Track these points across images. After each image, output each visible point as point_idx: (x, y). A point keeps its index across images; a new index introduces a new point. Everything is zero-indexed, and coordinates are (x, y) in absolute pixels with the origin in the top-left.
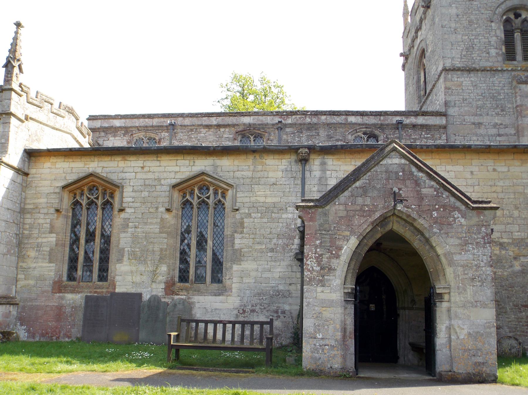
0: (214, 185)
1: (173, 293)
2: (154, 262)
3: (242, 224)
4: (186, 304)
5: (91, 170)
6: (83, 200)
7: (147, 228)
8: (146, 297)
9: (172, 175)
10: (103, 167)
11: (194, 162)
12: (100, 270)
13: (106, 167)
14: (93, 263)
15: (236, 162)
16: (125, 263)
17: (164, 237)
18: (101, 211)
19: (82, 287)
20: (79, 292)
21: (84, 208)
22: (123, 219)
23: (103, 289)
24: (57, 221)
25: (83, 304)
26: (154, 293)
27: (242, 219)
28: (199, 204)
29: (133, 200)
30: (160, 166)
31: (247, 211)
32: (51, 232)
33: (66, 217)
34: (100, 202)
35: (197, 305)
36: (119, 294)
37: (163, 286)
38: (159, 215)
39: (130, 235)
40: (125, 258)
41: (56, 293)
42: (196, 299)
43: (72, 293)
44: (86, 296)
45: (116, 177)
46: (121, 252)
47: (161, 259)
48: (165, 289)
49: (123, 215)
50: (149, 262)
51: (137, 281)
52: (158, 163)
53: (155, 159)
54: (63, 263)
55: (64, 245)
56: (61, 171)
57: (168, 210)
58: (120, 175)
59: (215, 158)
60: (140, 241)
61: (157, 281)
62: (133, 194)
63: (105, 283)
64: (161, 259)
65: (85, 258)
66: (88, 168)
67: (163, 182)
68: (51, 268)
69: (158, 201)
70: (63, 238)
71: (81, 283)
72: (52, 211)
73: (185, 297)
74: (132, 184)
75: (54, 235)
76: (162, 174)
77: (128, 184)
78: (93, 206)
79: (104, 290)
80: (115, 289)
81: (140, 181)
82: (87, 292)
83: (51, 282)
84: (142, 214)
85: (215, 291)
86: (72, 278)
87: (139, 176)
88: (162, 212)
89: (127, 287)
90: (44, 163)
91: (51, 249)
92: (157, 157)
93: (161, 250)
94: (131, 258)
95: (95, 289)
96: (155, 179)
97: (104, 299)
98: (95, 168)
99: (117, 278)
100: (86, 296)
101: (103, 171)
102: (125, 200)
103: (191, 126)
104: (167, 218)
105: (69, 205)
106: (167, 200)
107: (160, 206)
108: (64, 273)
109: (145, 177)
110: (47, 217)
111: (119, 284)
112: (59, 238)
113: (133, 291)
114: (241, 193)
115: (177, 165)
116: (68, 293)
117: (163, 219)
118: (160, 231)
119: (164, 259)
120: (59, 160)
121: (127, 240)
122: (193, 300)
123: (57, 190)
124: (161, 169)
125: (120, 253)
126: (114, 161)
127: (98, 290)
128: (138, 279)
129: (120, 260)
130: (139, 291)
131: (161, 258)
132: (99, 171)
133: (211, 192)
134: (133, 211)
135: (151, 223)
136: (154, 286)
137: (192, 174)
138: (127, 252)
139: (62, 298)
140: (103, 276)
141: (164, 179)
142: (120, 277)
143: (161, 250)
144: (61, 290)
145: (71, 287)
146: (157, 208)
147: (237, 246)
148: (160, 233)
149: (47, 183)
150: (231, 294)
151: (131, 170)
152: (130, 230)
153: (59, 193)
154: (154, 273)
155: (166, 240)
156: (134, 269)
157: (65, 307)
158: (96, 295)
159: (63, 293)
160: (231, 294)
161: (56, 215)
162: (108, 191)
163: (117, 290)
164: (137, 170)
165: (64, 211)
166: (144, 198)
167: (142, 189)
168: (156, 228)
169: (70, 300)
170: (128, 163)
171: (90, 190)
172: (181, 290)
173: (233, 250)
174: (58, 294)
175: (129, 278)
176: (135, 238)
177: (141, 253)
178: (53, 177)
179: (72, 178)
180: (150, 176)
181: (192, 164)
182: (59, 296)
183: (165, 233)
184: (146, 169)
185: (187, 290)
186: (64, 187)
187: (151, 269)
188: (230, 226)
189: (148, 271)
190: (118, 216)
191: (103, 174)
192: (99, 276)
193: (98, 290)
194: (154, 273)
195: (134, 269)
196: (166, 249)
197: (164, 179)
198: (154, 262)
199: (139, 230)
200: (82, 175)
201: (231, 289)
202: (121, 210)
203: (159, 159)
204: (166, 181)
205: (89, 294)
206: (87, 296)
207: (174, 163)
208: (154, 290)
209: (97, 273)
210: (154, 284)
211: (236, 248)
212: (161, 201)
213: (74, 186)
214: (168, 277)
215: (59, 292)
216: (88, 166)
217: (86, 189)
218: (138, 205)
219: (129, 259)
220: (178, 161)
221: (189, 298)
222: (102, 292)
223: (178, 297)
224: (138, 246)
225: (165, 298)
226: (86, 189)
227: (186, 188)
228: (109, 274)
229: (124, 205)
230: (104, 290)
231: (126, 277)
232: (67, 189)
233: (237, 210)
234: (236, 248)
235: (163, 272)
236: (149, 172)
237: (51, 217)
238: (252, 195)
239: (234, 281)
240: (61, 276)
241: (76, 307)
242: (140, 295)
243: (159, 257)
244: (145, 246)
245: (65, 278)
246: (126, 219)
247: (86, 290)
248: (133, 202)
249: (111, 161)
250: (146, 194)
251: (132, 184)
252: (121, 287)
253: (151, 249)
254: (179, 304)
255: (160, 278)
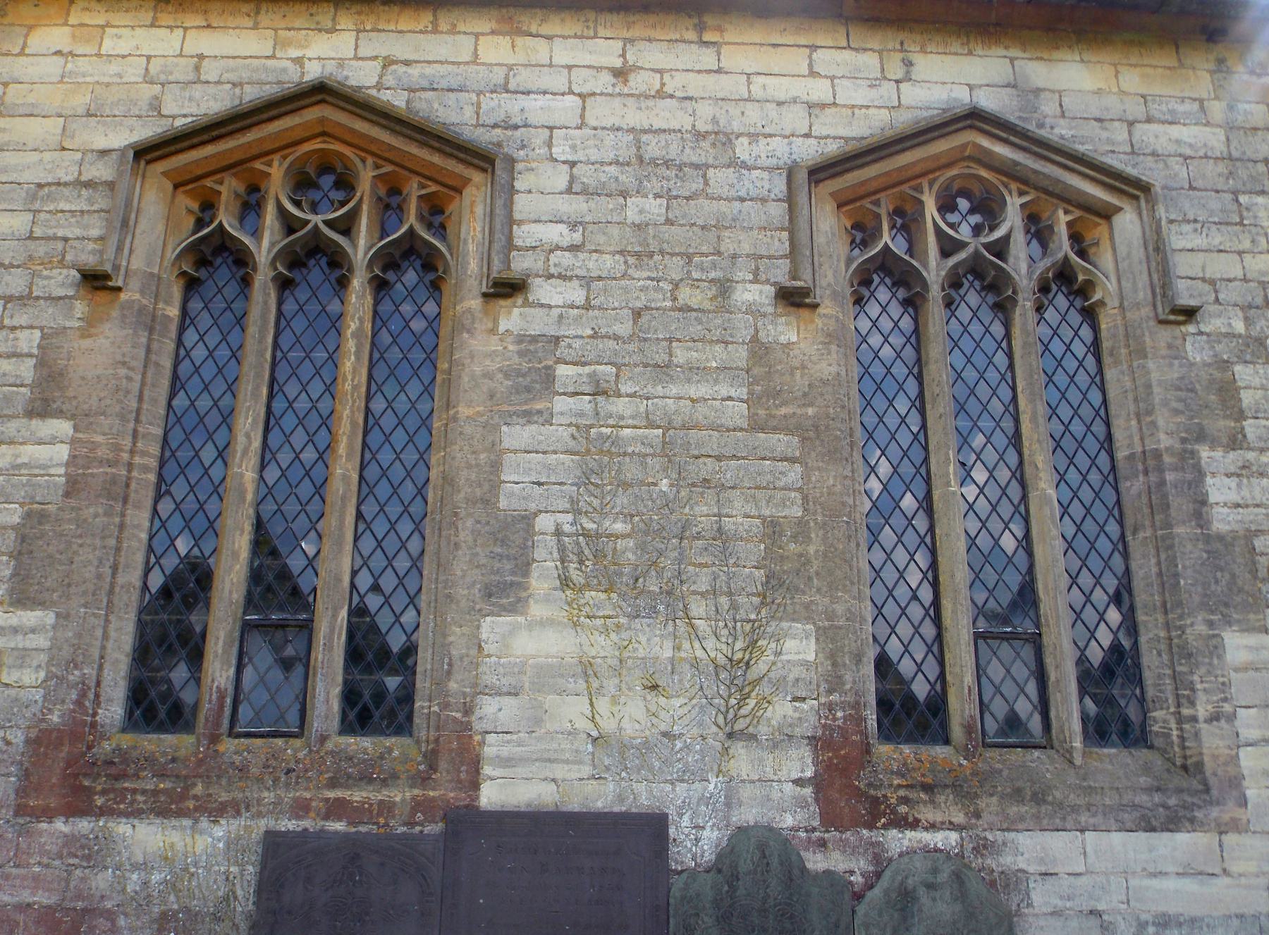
0: (1023, 180)
1: (876, 812)
2: (734, 607)
3: (1228, 391)
4: (974, 886)
5: (313, 72)
6: (256, 234)
7: (672, 397)
8: (696, 841)
9: (795, 119)
10: (388, 62)
11: (909, 64)
12: (354, 655)
13: (407, 63)
14: (309, 608)
15: (1132, 80)
16: (537, 610)
17: (780, 449)
18: (369, 300)
19: (243, 769)
20: (218, 812)
21: (263, 277)
22: (520, 339)
23: (386, 791)
24: (86, 343)
25: (245, 900)
26: (748, 815)
27: (1225, 365)
28: (954, 282)
29: (577, 237)
30: (719, 71)
31: (1239, 327)
32: (41, 408)
33: (150, 322)
34: (361, 248)
35: (1041, 897)
36: (505, 820)
37: (800, 762)
38: (743, 328)
39: (564, 433)
40: (541, 580)
41: (48, 814)
42: (1028, 849)
43: (163, 813)
44: (270, 835)
45: (469, 112)
46: (513, 538)
47: (778, 589)
48: (818, 783)
49: (513, 318)
50: (698, 608)
51: (629, 729)
52: (707, 58)
53: (691, 35)
54: (110, 607)
55: (120, 493)
56: (133, 71)
57: (793, 298)
58: (488, 102)
59: (1014, 52)
60: (632, 471)
61: (763, 731)
62: (576, 206)
63: (395, 745)
64: (778, 589)
65: (255, 576)
66: (299, 61)
67: (743, 149)
68: (19, 641)
69: (728, 246)
70: (117, 448)
71: (228, 746)
72: (61, 281)
73: (954, 837)
74: (561, 151)
75: (63, 427)
76: (735, 111)
77: (543, 151)
78: (316, 273)
79: (400, 795)
80: (475, 786)
81: (610, 138)
82: (276, 809)
83: (18, 737)
84: (637, 314)
85: (1143, 799)
86: (162, 711)
87: (600, 112)
88: (752, 310)
89: (560, 772)
90: (31, 28)
91: (36, 517)
92: (701, 28)
93: (773, 529)
94: (576, 576)
95: (333, 784)
96: (700, 136)
97: (399, 856)
98: (341, 63)
99: (489, 708)
100: (268, 833)
101: (389, 80)
102: (525, 234)
103: (97, 696)
104: (788, 345)
105: (171, 255)
106: (780, 243)
107: (740, 275)
108: (108, 675)
109: (635, 118)
110: (22, 319)
111: (505, 751)
112: (94, 446)
113: (602, 796)
114: (1187, 228)
115: (813, 74)
116: (136, 813)
117: (767, 349)
118: (752, 417)
119: (793, 590)
120: (119, 18)
121: (549, 468)
122: (1007, 860)
123: (102, 171)
124: (731, 85)
125: (503, 542)
126: (453, 31)
127: (357, 796)
128: (631, 716)
129: (505, 593)
130: (643, 795)
131: (773, 582)
132: (362, 77)
133: (1012, 219)
134: (578, 296)
135: (695, 371)
136: (743, 761)
137: (904, 120)
138: (551, 541)
139: (90, 854)
140: (380, 694)
141: (753, 137)
142: (508, 701)
143: (773, 529)
144: (89, 792)
145: (162, 775)
146: (724, 288)
147: (1223, 521)
148: (756, 426)
149: (43, 130)
150: (1239, 813)
151: (558, 81)
152: (561, 404)
153: (111, 185)
154: (738, 677)
155: (794, 474)
156: (602, 646)
157: (110, 915)
158: (339, 826)
159: (103, 812)
160: (1239, 813)
161: (80, 308)
162: (413, 190)
163: (491, 796)
164: (584, 81)
165: (135, 284)
166: (638, 227)
167: (627, 178)
168: (727, 401)
169: (144, 867)
170: (539, 50)
171: (302, 183)
172: (928, 788)
173: (1208, 539)
174: (60, 825)
175: (571, 711)
176: (597, 457)
177: (642, 547)
178: (80, 101)
179: (190, 106)
180: (666, 115)
181: (896, 71)
182: (70, 840)
183: (789, 431)
184: (638, 82)
185: (963, 789)
186: (146, 153)
187: (714, 649)
188: (1165, 403)
189: (695, 664)
190: (483, 325)
191: (386, 96)
192: (350, 696)
193: (357, 796)
194: (738, 677)
195: (602, 646)
196: (801, 531)
197: (753, 137)
198: (734, 607)
199: (620, 406)
200: (252, 94)
201: (1235, 782)
202: (507, 288)
203: (707, 37)
204: (762, 148)
205: (288, 825)
206: (273, 841)
207: (797, 61)
208: (746, 792)
209: (340, 679)
210: (739, 749)
211: (1219, 526)
212: (746, 248)
213: (209, 150)
214: (831, 707)
215: (72, 811)
216: (295, 53)
217: (277, 174)
218: (609, 263)
219: (565, 582)
220: (819, 55)
221: (983, 847)
222: (386, 808)
223: (911, 838)
224: (622, 500)
225: (822, 844)
226: (277, 174)
227: (871, 192)
228: (423, 684)
229: (521, 264)
230: (400, 795)
231: (551, 700)
232: (161, 167)
233: (1190, 314)
234: (1219, 526)
235: (796, 672)
236: (661, 94)
237: (50, 316)
238: (1247, 244)
239: (1248, 733)
240: (90, 694)
241: (193, 916)
242: (653, 828)
243: (760, 574)
244: (667, 504)
245: (113, 710)
246: (534, 339)
247: (268, 796)
248: (573, 248)
249: (435, 31)
250: (655, 207)
251: (561, 151)
252: (521, 771)
253: (705, 523)
254: (930, 886)
255: (781, 710)
